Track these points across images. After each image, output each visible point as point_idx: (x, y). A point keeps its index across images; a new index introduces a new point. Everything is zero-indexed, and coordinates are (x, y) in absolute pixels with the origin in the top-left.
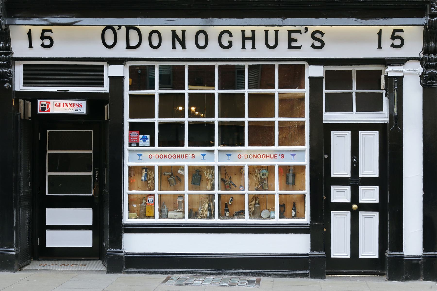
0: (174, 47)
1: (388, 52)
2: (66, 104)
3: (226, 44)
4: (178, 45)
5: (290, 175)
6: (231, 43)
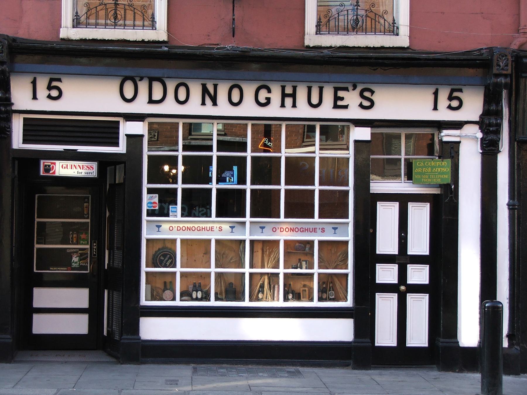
0: (203, 103)
1: (444, 114)
2: (74, 165)
3: (262, 100)
4: (208, 101)
5: (332, 250)
6: (268, 100)
